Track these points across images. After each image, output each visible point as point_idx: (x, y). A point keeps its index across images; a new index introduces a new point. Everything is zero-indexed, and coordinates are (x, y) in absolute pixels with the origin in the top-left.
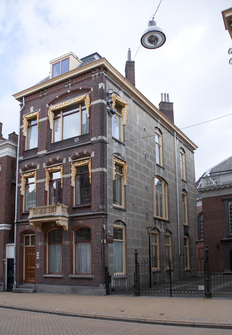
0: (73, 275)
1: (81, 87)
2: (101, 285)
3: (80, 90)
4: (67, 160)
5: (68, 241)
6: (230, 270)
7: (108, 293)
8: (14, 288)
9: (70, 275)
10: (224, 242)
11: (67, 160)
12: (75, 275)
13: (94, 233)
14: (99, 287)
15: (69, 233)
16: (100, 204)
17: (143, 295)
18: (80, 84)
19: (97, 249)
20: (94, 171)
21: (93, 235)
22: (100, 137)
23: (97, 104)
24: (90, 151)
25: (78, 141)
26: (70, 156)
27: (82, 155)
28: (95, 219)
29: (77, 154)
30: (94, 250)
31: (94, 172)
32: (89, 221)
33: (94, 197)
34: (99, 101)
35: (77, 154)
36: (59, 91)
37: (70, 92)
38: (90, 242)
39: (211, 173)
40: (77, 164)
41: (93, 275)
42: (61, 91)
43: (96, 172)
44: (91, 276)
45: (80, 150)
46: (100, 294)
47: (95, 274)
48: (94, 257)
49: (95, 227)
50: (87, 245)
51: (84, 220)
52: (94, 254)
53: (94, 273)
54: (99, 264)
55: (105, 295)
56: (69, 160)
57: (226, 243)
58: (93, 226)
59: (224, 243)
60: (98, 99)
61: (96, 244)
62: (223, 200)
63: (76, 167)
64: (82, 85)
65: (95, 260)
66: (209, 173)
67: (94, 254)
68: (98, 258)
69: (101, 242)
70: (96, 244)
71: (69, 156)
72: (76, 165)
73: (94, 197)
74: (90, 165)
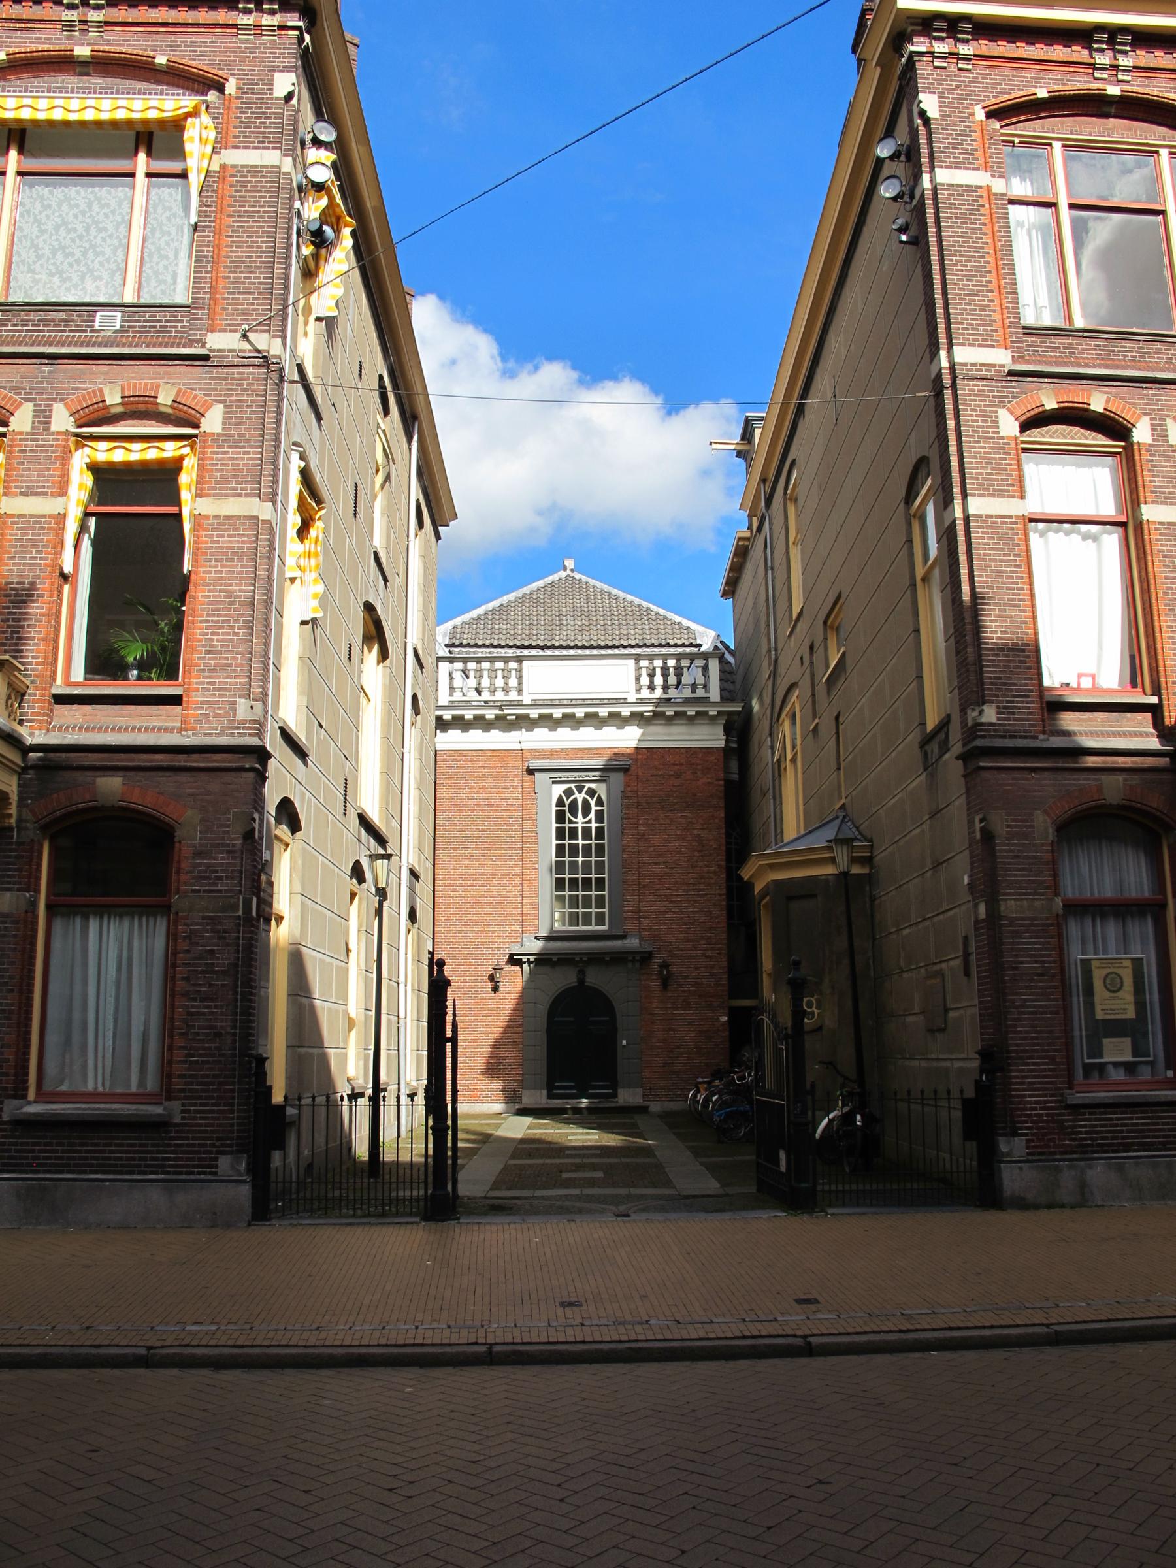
0: (29, 1103)
1: (163, 53)
2: (224, 1163)
3: (153, 64)
4: (43, 417)
5: (8, 894)
6: (545, 1092)
7: (261, 1212)
8: (1015, 1178)
9: (15, 1102)
10: (634, 960)
11: (43, 417)
12: (35, 1102)
13: (199, 854)
14: (215, 1173)
15: (23, 843)
16: (241, 697)
17: (283, 1214)
18: (159, 38)
19: (212, 951)
20: (207, 506)
21: (185, 866)
22: (261, 340)
23: (255, 170)
24: (196, 399)
25: (116, 332)
26: (62, 400)
27: (140, 408)
28: (203, 776)
29: (113, 398)
30: (188, 951)
31: (217, 517)
32: (167, 783)
33: (209, 652)
34: (271, 157)
35: (113, 398)
36: (15, 30)
37: (92, 57)
38: (169, 907)
39: (453, 645)
40: (104, 453)
41: (176, 1105)
42: (28, 30)
43: (228, 517)
44: (159, 1110)
45: (140, 379)
46: (218, 1220)
47: (186, 1098)
48: (185, 994)
49: (202, 820)
50: (144, 919)
51: (132, 773)
52: (187, 979)
53: (183, 1090)
54: (218, 1035)
55: (249, 1225)
56: (53, 420)
57: (637, 965)
58: (189, 813)
59: (630, 965)
60: (261, 145)
61: (204, 918)
62: (531, 772)
63: (95, 468)
64: (173, 48)
65: (189, 1014)
66: (447, 646)
67: (187, 979)
68: (212, 1000)
69: (235, 907)
70: (204, 918)
71: (55, 400)
72: (102, 457)
73: (209, 652)
74: (186, 479)
